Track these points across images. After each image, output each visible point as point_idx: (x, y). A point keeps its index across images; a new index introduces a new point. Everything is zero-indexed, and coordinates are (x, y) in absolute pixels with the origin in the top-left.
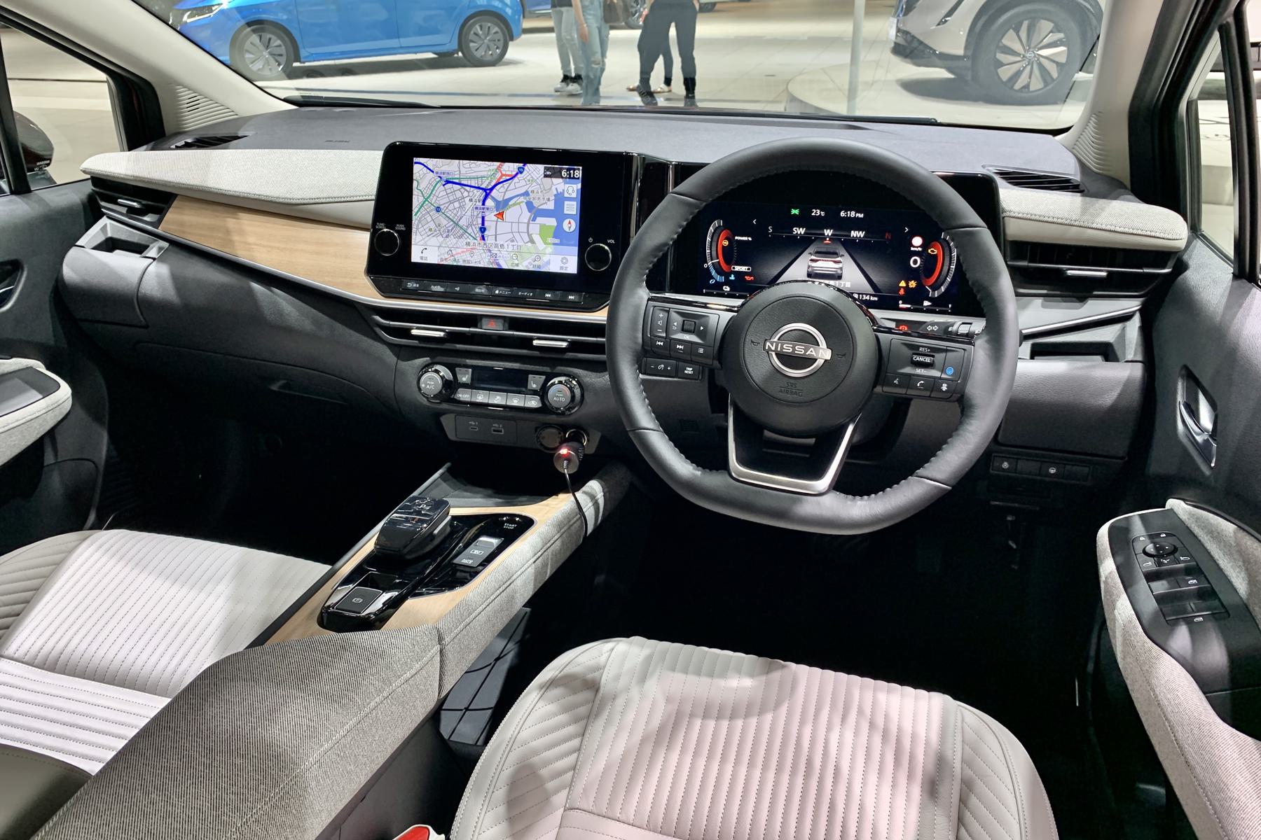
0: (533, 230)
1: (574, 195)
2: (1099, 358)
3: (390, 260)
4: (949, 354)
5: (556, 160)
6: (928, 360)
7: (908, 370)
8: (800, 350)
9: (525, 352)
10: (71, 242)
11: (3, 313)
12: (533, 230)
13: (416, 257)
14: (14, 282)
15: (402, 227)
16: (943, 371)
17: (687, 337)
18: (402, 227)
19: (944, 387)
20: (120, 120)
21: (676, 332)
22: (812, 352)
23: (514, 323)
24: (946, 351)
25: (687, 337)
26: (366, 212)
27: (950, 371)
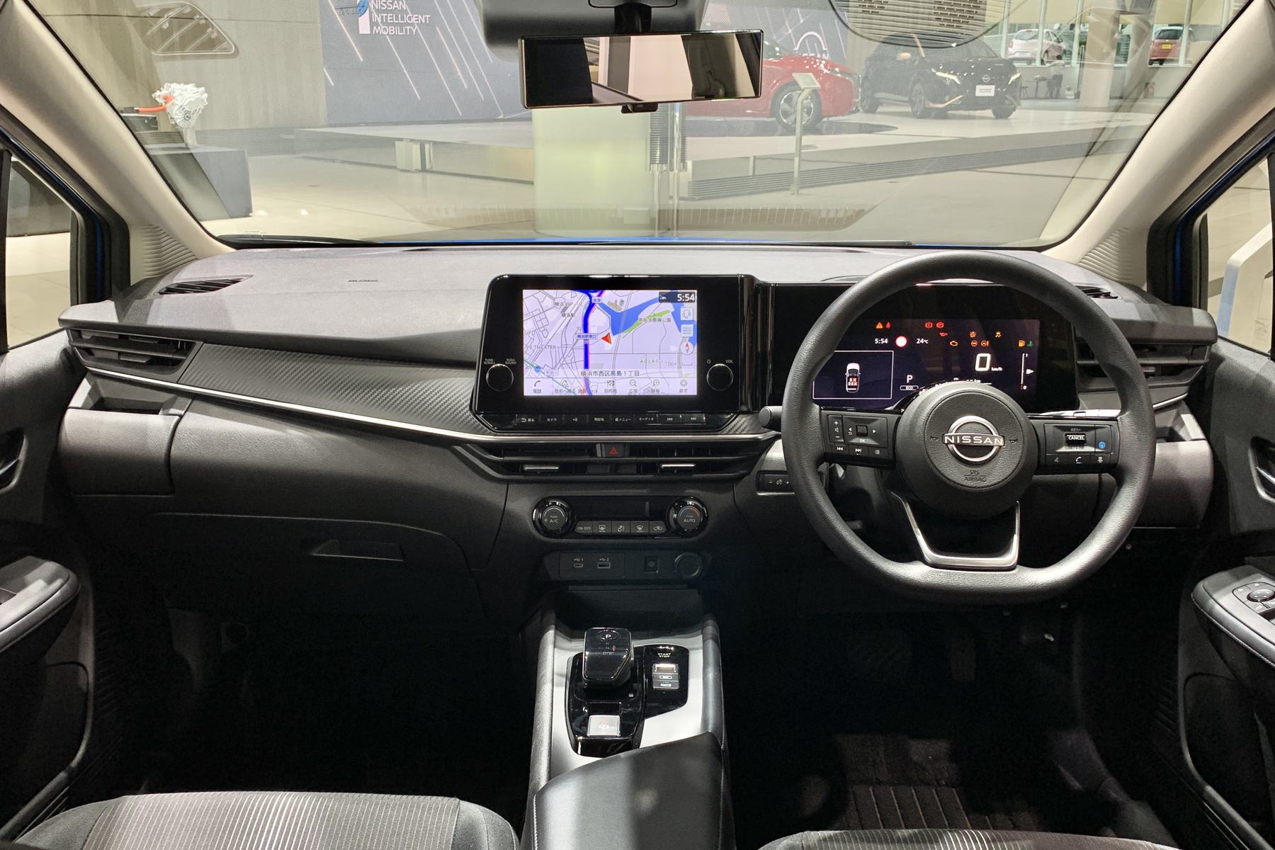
0: (659, 359)
1: (690, 318)
2: (29, 558)
3: (500, 395)
4: (1098, 431)
5: (670, 284)
6: (1081, 437)
7: (1064, 449)
8: (978, 441)
9: (650, 476)
10: (65, 407)
11: (3, 495)
12: (659, 359)
13: (529, 390)
14: (15, 455)
15: (512, 361)
16: (1096, 446)
17: (862, 441)
18: (512, 361)
19: (1100, 460)
20: (1051, 277)
21: (852, 437)
22: (988, 441)
23: (635, 449)
24: (1095, 428)
25: (862, 441)
26: (475, 349)
27: (1102, 445)
